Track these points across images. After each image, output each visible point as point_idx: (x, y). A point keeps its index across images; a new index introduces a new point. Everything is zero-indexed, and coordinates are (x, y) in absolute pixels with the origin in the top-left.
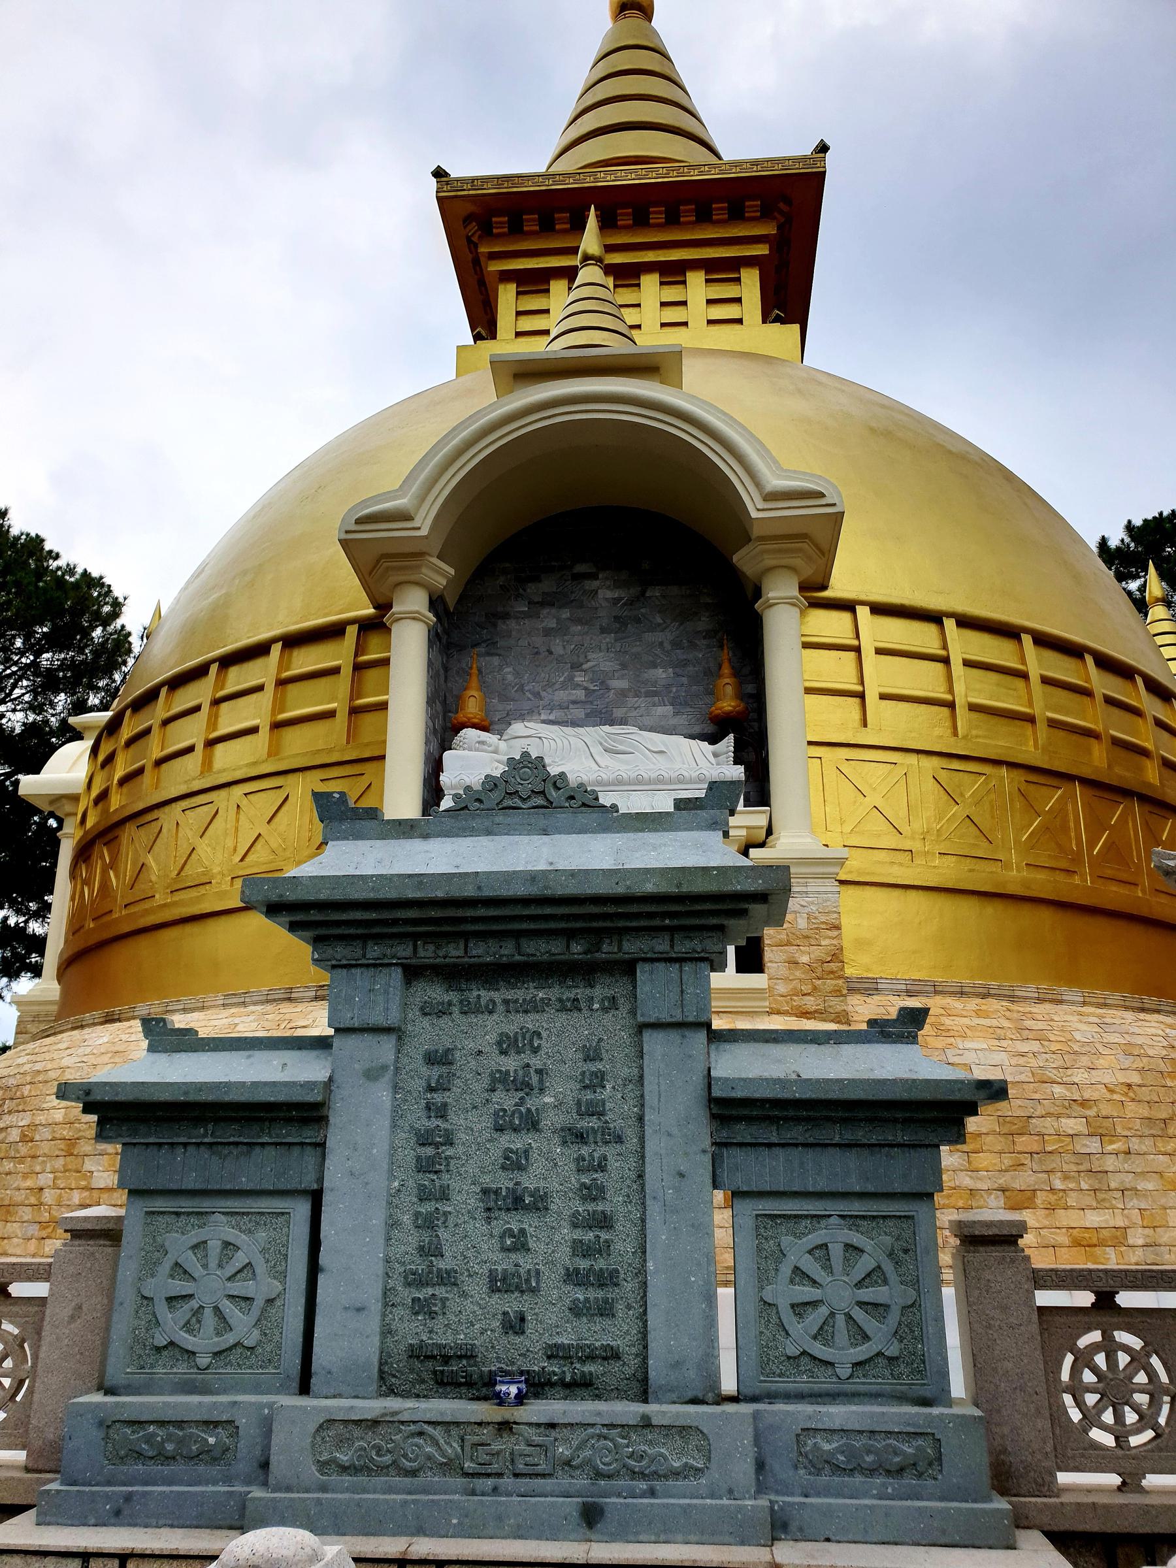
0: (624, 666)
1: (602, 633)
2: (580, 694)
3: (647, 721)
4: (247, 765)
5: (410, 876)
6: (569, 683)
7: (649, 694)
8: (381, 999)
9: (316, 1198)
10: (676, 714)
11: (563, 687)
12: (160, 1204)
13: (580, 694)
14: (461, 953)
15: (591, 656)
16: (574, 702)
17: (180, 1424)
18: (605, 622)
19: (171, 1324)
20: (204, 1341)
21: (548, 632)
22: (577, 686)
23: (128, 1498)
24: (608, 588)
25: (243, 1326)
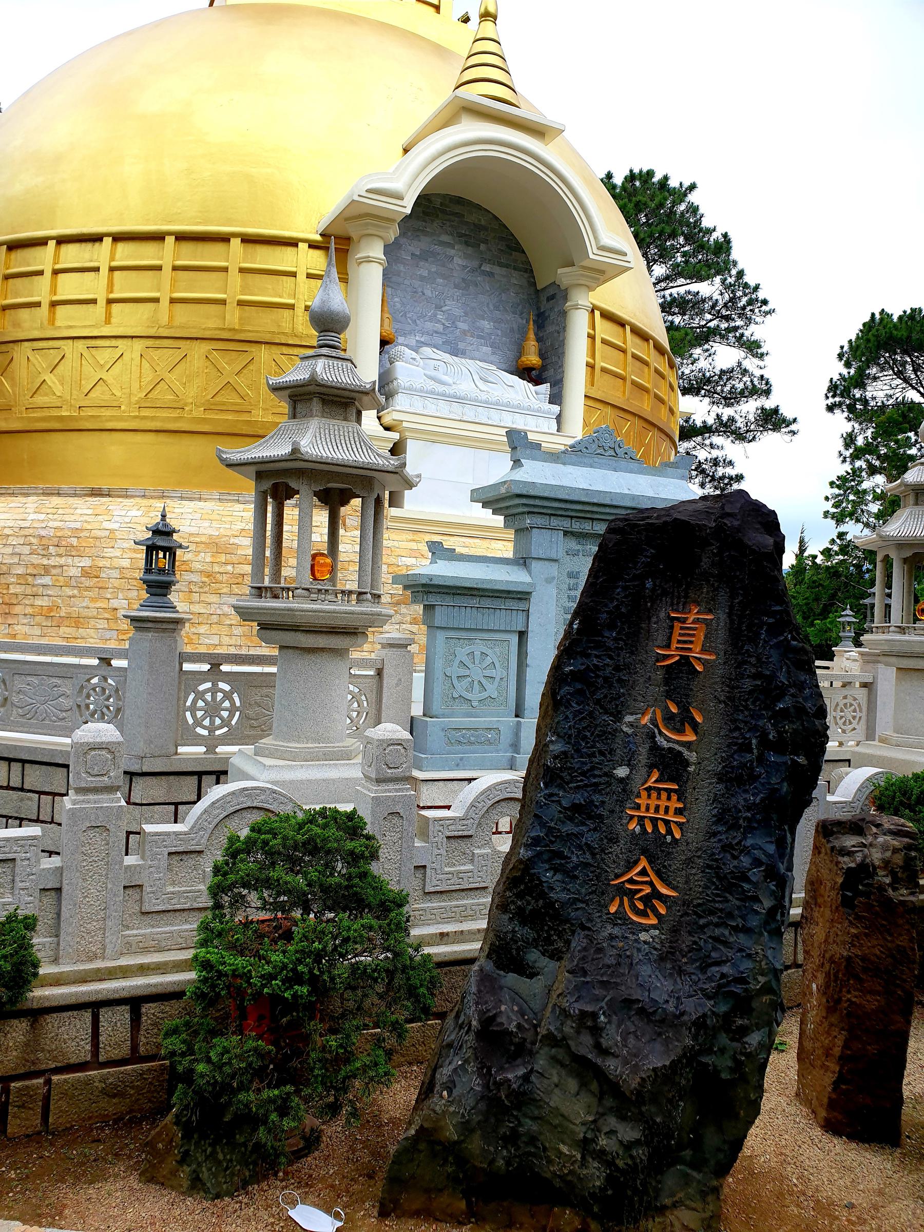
0: (466, 314)
1: (455, 288)
2: (439, 327)
3: (477, 354)
4: (216, 329)
5: (583, 489)
6: (433, 319)
7: (479, 337)
8: (555, 546)
9: (522, 635)
10: (493, 353)
11: (431, 320)
12: (452, 634)
13: (439, 327)
14: (569, 525)
15: (448, 302)
16: (436, 332)
17: (476, 729)
18: (457, 281)
19: (461, 687)
20: (475, 696)
21: (422, 278)
22: (438, 321)
23: (461, 759)
24: (460, 257)
25: (492, 689)
